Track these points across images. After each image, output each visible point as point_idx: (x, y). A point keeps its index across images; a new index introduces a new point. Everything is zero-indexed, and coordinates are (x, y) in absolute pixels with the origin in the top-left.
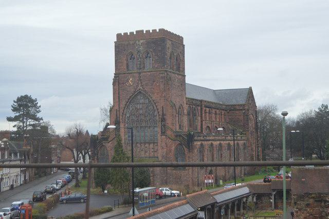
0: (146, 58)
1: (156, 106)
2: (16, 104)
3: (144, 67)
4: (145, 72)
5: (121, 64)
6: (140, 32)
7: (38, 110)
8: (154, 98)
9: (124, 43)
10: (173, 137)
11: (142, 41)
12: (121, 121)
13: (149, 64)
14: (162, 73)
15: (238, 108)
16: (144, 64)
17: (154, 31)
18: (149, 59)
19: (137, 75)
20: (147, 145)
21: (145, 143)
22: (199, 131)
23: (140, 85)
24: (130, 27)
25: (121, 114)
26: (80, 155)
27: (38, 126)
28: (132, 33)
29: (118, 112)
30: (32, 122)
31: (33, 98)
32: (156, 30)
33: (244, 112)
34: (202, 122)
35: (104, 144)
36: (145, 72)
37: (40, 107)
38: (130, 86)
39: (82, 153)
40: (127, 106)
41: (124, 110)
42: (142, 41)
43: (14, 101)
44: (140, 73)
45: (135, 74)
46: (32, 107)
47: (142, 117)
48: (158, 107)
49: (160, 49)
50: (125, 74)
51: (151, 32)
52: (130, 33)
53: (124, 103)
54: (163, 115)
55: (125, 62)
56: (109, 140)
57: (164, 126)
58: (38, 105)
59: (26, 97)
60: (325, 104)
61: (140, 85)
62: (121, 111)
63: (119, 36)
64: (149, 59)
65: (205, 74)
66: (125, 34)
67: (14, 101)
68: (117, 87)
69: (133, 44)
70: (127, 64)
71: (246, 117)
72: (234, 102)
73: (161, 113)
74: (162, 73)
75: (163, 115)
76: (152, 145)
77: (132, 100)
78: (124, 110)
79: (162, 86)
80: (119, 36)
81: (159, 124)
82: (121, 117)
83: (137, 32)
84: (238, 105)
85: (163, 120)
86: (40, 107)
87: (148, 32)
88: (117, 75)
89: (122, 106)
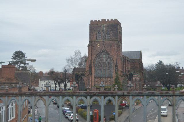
0: (107, 33)
1: (113, 59)
2: (14, 55)
3: (106, 38)
4: (106, 41)
5: (93, 36)
6: (104, 20)
7: (26, 59)
8: (111, 55)
9: (94, 25)
10: (122, 75)
11: (105, 25)
12: (92, 66)
13: (108, 37)
14: (116, 42)
15: (136, 61)
16: (106, 37)
17: (112, 20)
18: (106, 33)
19: (102, 42)
20: (106, 79)
21: (105, 78)
22: (125, 72)
23: (103, 48)
24: (99, 17)
25: (93, 62)
26: (57, 83)
27: (178, 70)
28: (99, 21)
29: (91, 61)
30: (22, 65)
31: (23, 53)
32: (105, 20)
33: (139, 63)
34: (126, 67)
35: (82, 78)
36: (106, 41)
37: (27, 57)
38: (98, 48)
39: (58, 82)
40: (96, 58)
41: (94, 60)
42: (105, 25)
43: (13, 54)
44: (103, 41)
45: (100, 42)
46: (23, 57)
47: (104, 64)
48: (114, 59)
49: (115, 29)
50: (95, 41)
51: (106, 20)
52: (98, 20)
53: (94, 56)
54: (117, 63)
55: (95, 35)
56: (86, 75)
57: (117, 69)
58: (26, 56)
59: (20, 52)
60: (161, 60)
61: (103, 48)
62: (93, 61)
63: (92, 21)
64: (106, 33)
65: (128, 46)
66: (95, 21)
67: (13, 54)
68: (90, 48)
69: (100, 26)
70: (96, 36)
71: (140, 65)
72: (133, 58)
73: (115, 62)
74: (116, 42)
75: (117, 63)
76: (109, 79)
77: (98, 55)
78: (94, 60)
79: (116, 49)
80: (92, 21)
81: (114, 68)
82: (92, 64)
83: (102, 20)
84: (137, 60)
85: (116, 66)
86: (27, 57)
87: (108, 20)
88: (90, 42)
89: (93, 58)
